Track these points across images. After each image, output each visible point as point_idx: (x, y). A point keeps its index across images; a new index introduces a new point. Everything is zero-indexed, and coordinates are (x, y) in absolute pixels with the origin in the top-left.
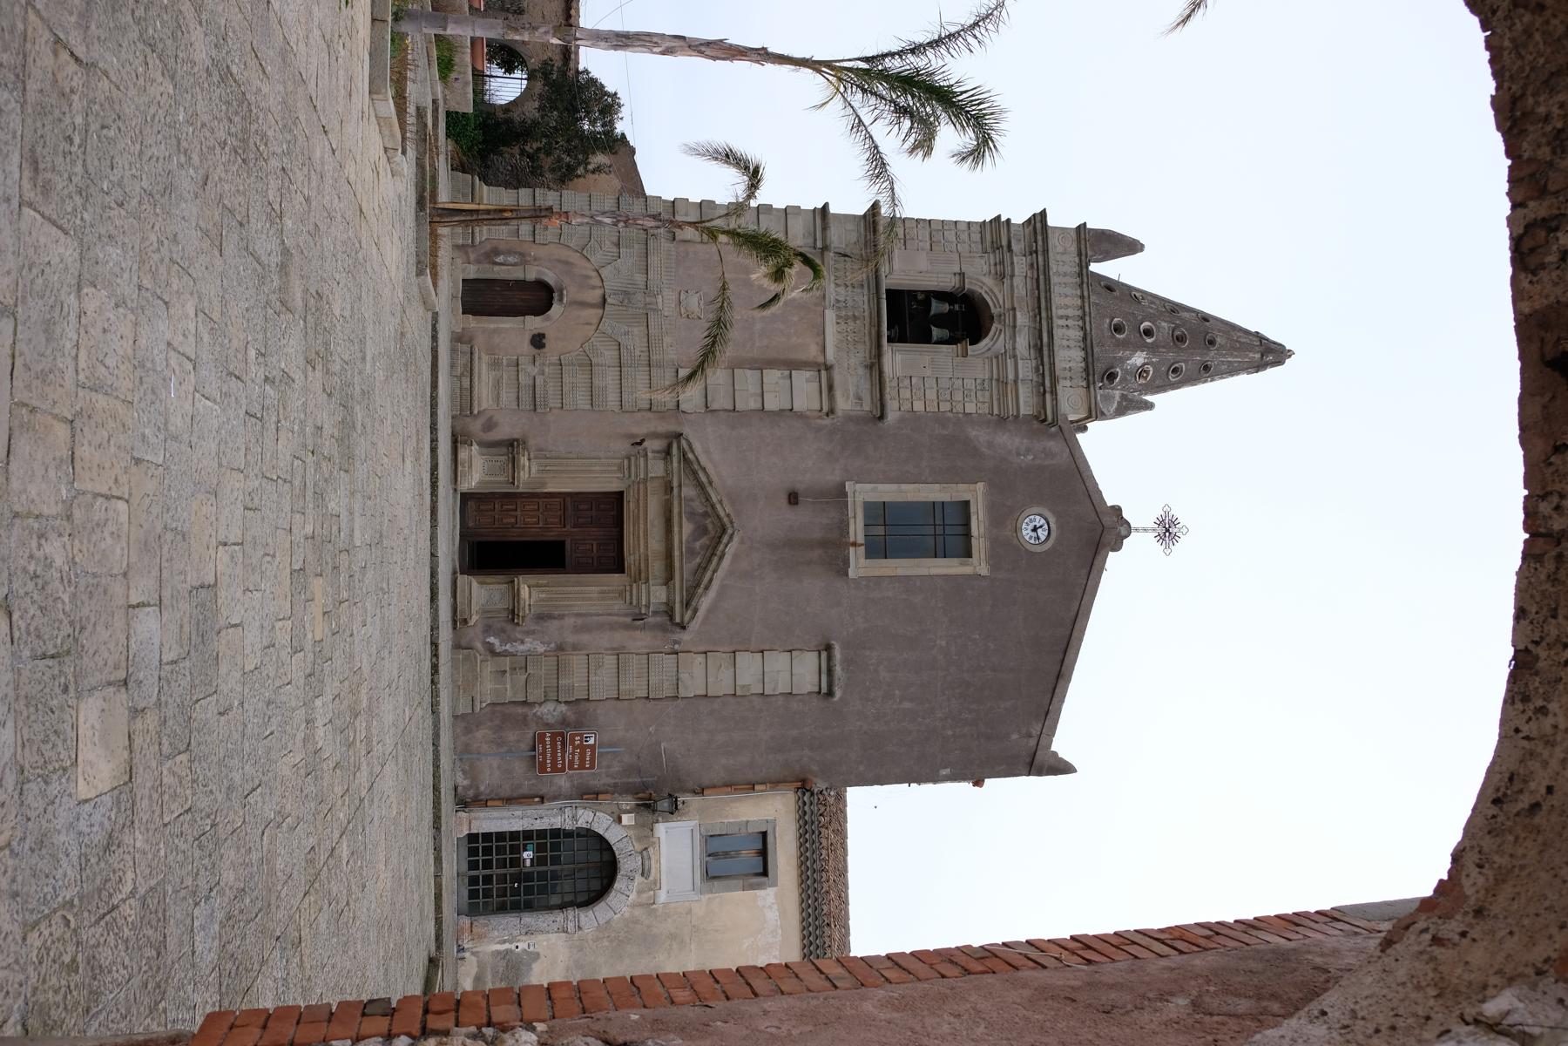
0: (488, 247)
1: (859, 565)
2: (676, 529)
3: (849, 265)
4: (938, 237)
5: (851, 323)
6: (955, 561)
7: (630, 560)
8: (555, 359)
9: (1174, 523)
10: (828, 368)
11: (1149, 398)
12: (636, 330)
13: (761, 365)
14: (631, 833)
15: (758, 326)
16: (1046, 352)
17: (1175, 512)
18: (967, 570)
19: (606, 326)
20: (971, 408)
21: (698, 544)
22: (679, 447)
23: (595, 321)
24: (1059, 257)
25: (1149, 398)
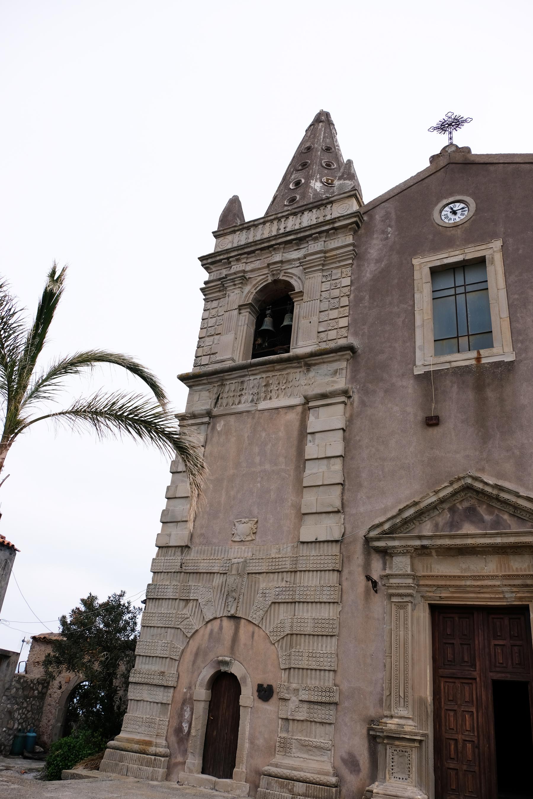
0: (173, 739)
1: (502, 351)
2: (469, 541)
3: (225, 395)
4: (212, 331)
5: (272, 387)
7: (510, 598)
8: (284, 675)
10: (307, 399)
12: (263, 585)
13: (301, 461)
15: (267, 467)
16: (302, 235)
18: (498, 258)
19: (256, 616)
20: (347, 281)
21: (487, 518)
22: (378, 539)
23: (251, 628)
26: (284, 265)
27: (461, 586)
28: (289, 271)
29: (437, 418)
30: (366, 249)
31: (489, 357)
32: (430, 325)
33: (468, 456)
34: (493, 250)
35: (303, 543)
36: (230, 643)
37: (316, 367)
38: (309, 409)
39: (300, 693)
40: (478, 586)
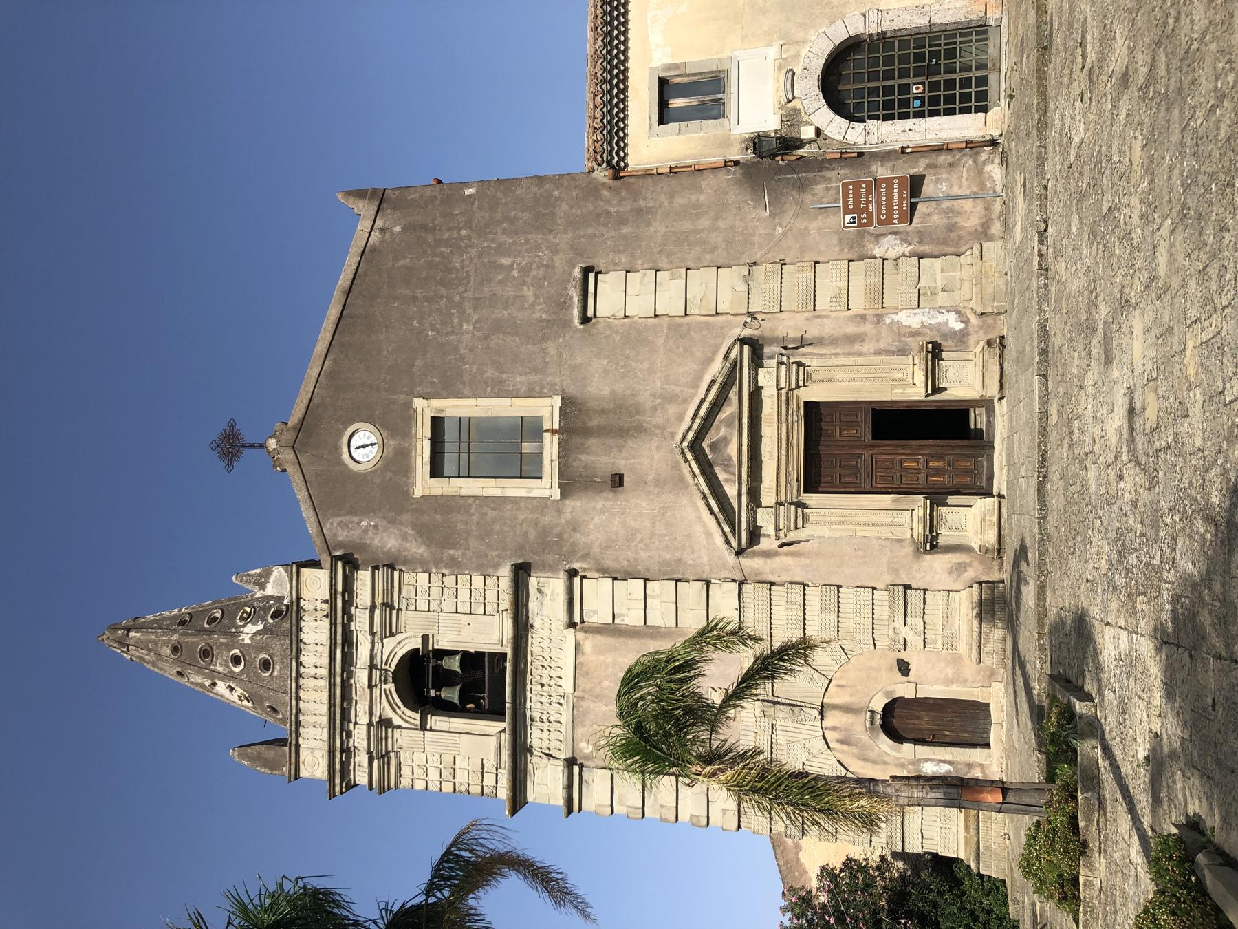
1: (548, 409)
10: (572, 624)
18: (437, 403)
29: (614, 476)
30: (384, 553)
33: (658, 448)
34: (425, 409)
36: (850, 715)
38: (582, 621)
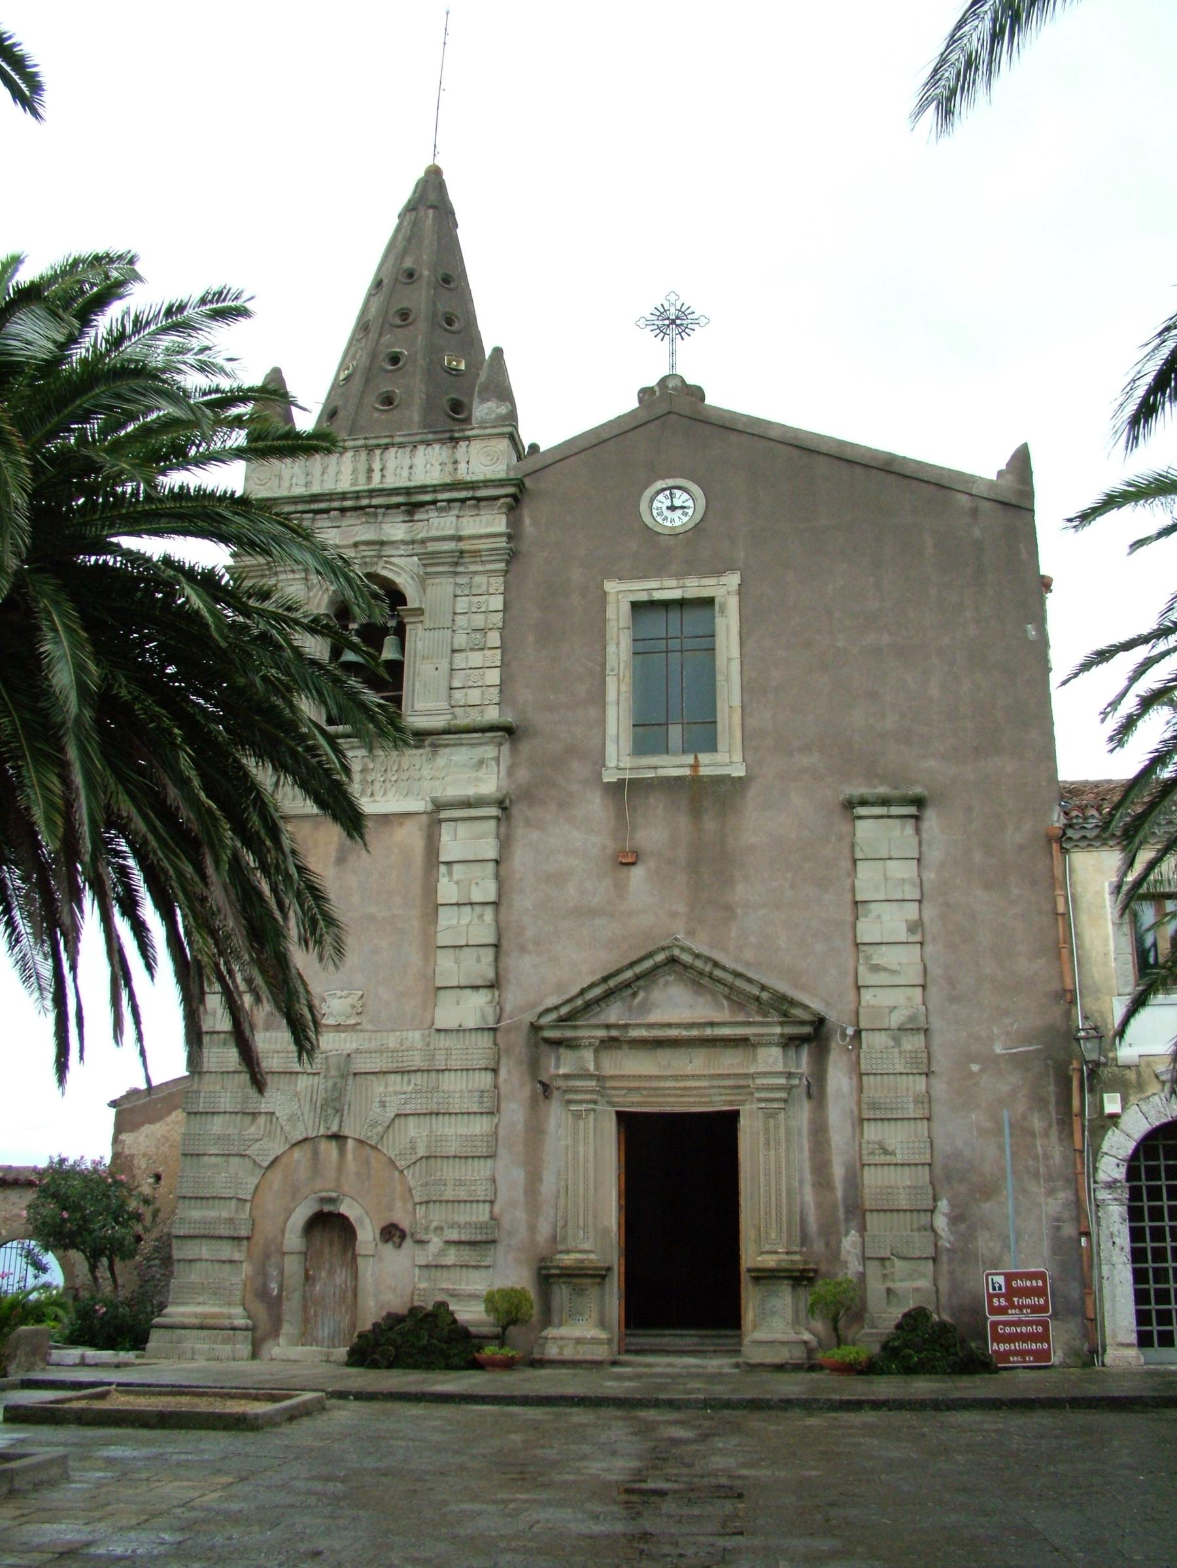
1: (727, 760)
6: (720, 621)
7: (718, 1103)
9: (662, 313)
11: (488, 352)
13: (432, 908)
14: (1133, 1099)
17: (647, 309)
18: (733, 603)
24: (286, 484)
25: (488, 352)
26: (385, 548)
27: (657, 1089)
28: (393, 560)
31: (711, 765)
32: (626, 705)
34: (725, 588)
35: (438, 1031)
37: (447, 750)
39: (446, 1232)
40: (679, 1088)
